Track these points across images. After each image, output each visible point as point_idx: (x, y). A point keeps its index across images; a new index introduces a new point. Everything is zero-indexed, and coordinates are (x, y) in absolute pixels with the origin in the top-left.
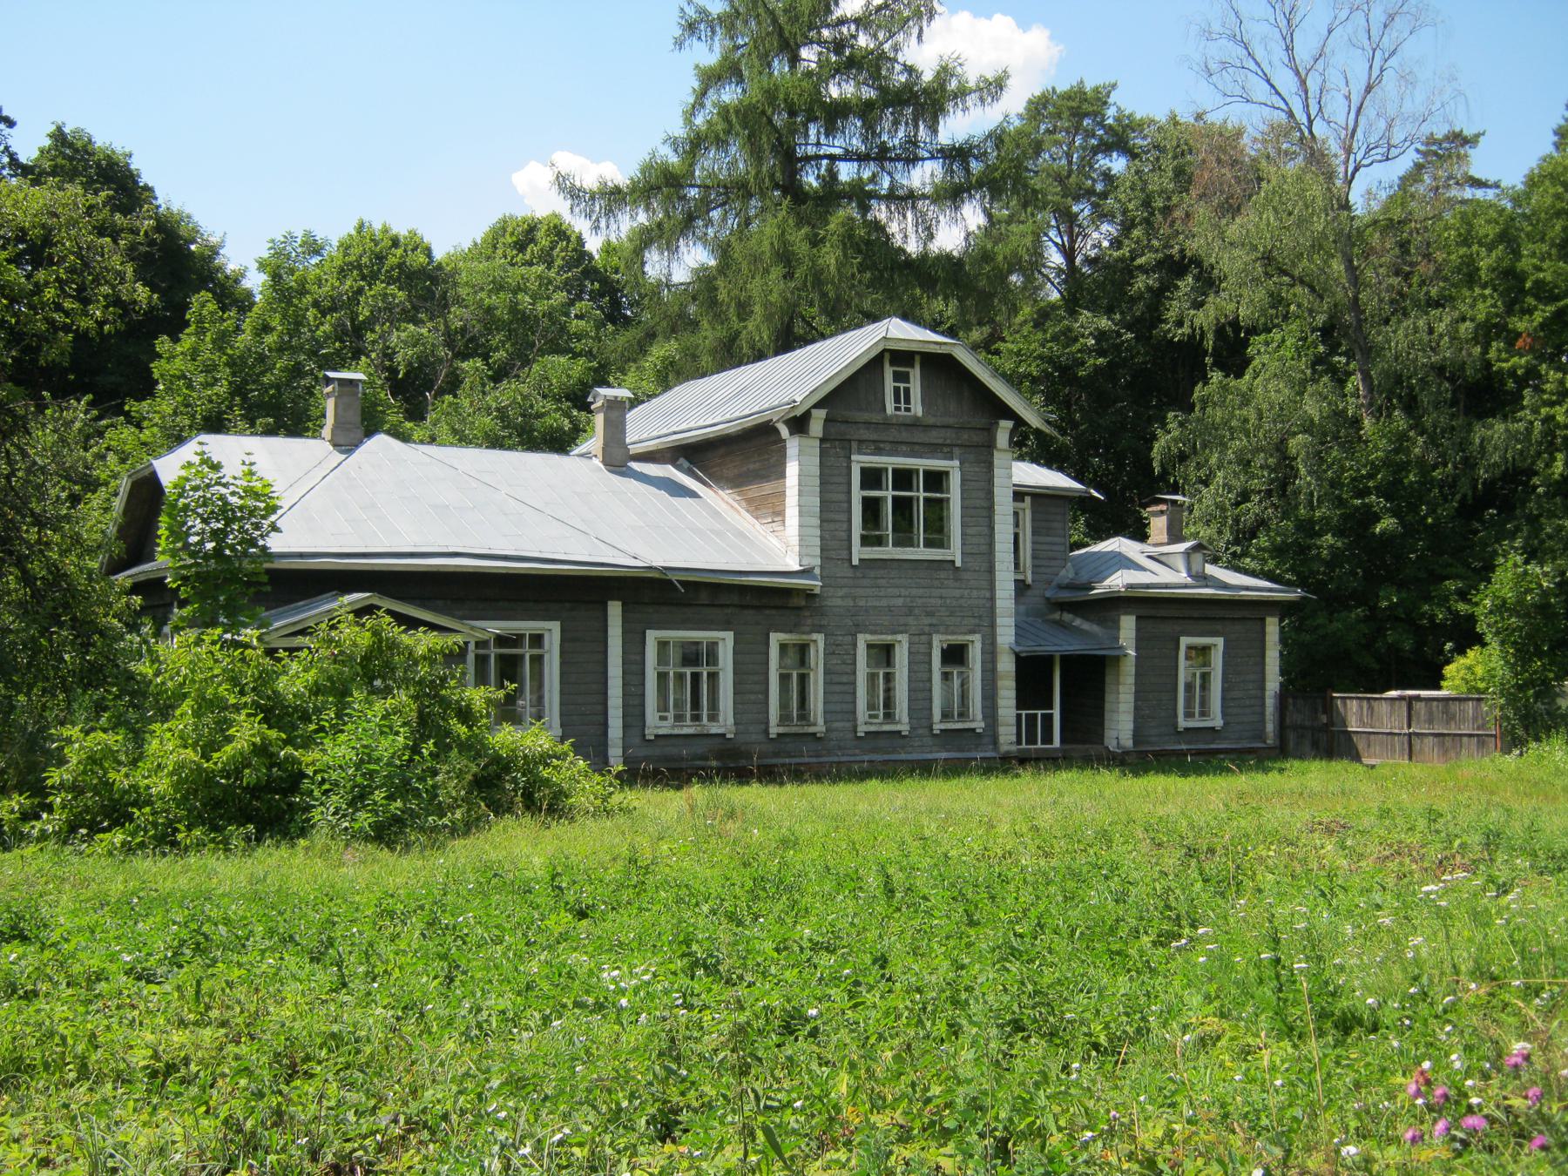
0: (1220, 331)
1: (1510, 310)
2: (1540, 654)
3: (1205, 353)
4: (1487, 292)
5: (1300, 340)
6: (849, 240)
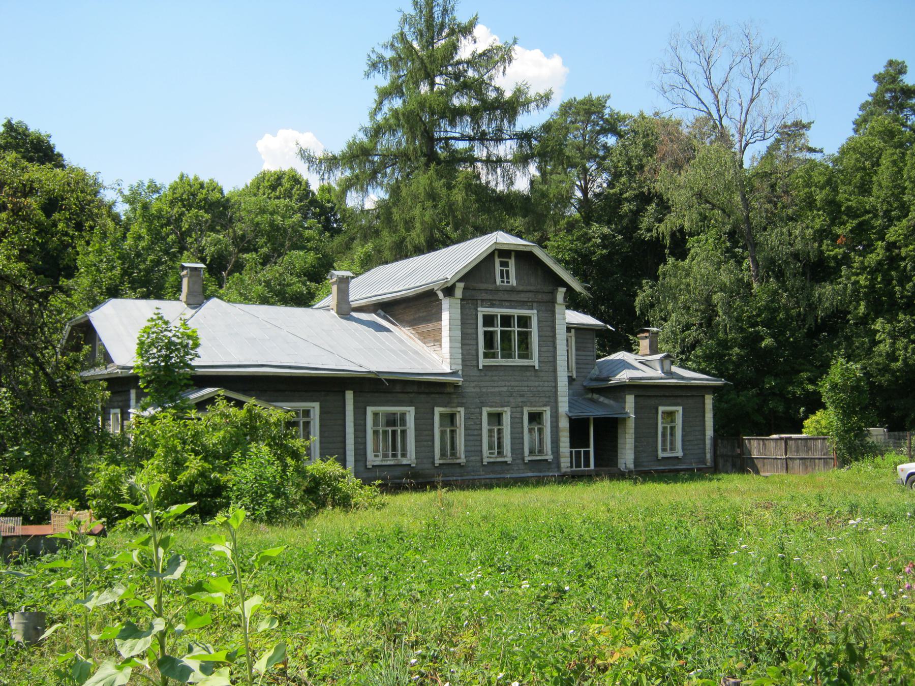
0: (673, 235)
1: (833, 223)
2: (855, 413)
3: (665, 247)
4: (820, 213)
5: (716, 239)
6: (468, 187)
